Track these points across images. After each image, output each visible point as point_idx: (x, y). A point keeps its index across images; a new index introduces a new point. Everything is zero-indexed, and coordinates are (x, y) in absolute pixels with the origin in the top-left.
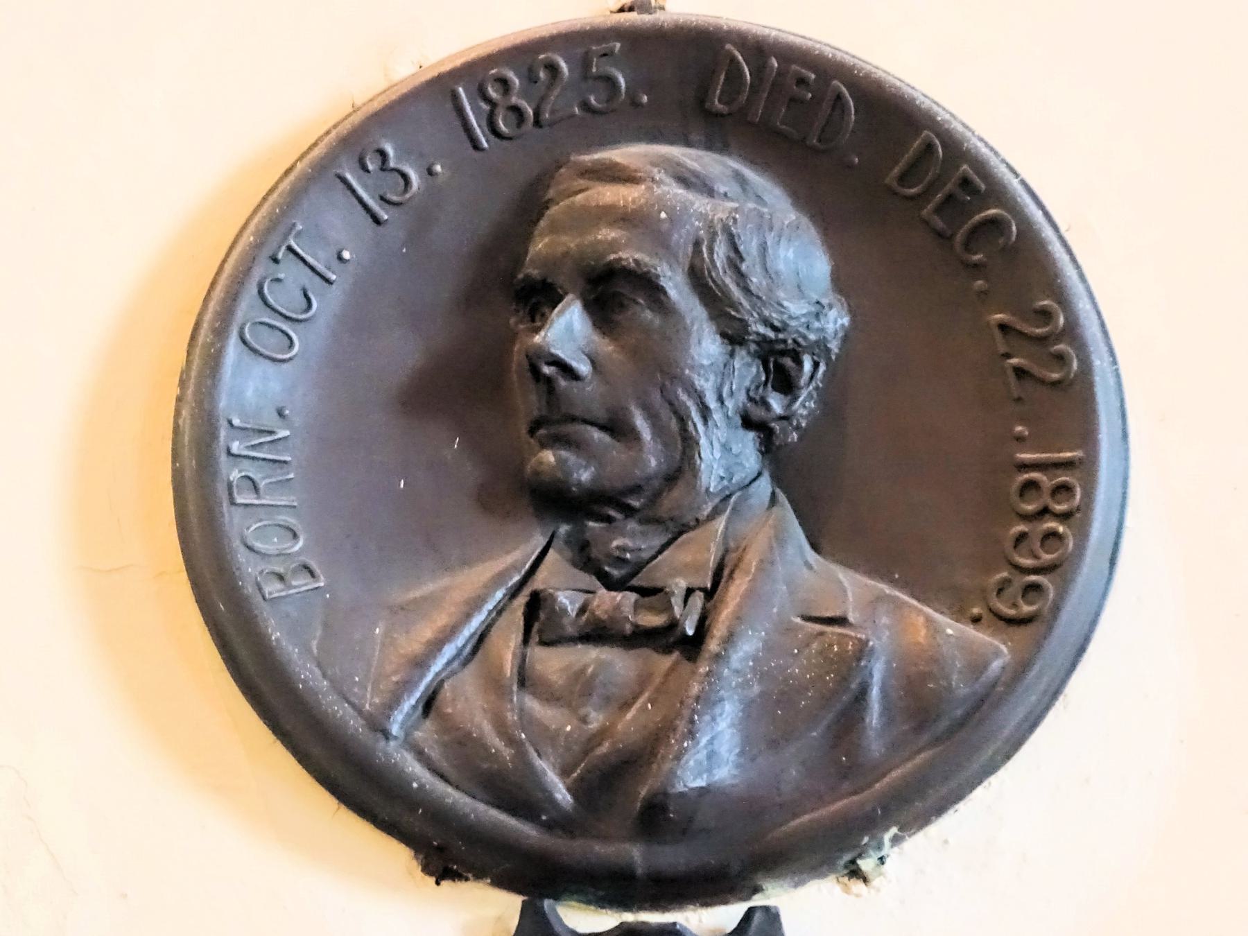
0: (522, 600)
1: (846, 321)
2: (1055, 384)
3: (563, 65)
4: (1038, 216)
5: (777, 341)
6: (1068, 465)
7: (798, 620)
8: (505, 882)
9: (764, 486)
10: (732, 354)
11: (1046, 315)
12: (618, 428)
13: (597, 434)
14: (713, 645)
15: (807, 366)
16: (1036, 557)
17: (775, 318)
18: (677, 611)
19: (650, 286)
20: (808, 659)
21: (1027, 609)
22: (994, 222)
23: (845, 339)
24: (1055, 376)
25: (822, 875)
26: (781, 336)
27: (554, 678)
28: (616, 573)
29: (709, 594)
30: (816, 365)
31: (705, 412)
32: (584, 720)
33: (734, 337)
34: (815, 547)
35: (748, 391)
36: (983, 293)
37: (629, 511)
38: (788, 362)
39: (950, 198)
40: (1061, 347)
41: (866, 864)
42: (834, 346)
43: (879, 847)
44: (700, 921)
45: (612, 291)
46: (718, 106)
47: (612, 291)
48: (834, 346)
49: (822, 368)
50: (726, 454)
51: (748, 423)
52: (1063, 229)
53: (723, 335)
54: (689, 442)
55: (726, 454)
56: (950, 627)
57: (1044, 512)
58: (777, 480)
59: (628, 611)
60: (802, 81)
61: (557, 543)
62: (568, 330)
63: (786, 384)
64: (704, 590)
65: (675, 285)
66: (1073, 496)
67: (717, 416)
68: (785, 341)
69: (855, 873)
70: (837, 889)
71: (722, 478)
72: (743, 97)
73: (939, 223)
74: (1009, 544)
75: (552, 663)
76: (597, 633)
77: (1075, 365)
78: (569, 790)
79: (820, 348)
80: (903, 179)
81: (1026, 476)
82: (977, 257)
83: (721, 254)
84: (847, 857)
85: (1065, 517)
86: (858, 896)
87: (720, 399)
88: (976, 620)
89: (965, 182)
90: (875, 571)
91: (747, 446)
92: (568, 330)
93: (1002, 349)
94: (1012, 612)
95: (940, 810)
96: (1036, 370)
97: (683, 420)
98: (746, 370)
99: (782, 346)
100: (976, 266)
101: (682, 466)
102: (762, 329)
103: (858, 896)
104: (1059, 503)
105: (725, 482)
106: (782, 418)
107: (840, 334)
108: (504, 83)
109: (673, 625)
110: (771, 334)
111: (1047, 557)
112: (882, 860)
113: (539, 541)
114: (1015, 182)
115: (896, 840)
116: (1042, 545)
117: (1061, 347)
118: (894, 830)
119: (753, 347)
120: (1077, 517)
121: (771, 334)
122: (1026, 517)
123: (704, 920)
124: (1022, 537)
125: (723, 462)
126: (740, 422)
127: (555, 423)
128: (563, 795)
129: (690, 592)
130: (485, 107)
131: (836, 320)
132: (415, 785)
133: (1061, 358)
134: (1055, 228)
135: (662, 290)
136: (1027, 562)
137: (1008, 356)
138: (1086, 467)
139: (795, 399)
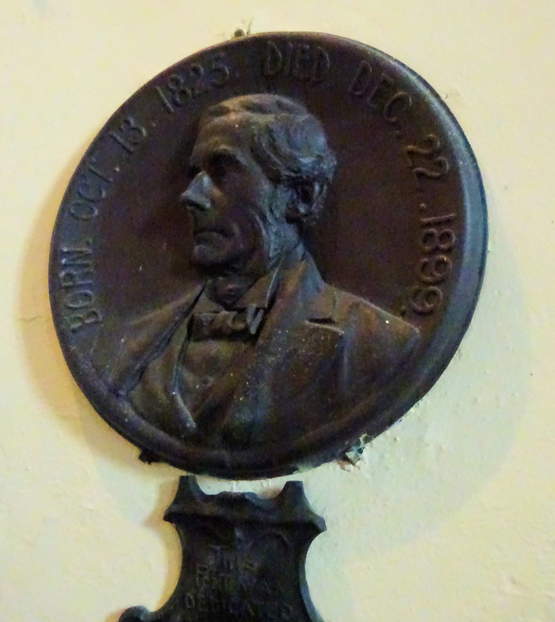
0: (187, 321)
1: (335, 162)
2: (436, 179)
3: (202, 70)
4: (427, 92)
5: (298, 178)
6: (449, 221)
7: (307, 322)
8: (174, 464)
9: (300, 250)
10: (276, 187)
11: (430, 142)
12: (225, 232)
13: (215, 234)
14: (261, 342)
15: (317, 188)
16: (432, 275)
17: (294, 167)
18: (249, 320)
19: (231, 160)
20: (310, 344)
21: (428, 306)
22: (399, 99)
23: (335, 173)
24: (437, 174)
25: (326, 460)
26: (299, 175)
27: (196, 358)
28: (229, 302)
29: (267, 311)
30: (322, 187)
31: (264, 218)
32: (205, 382)
33: (276, 180)
34: (324, 278)
35: (287, 204)
36: (399, 137)
37: (235, 270)
38: (307, 188)
39: (379, 90)
40: (441, 158)
41: (350, 455)
42: (330, 176)
43: (358, 443)
44: (268, 485)
45: (219, 165)
46: (270, 72)
47: (219, 165)
48: (330, 176)
49: (325, 187)
50: (277, 236)
51: (290, 220)
52: (443, 97)
53: (270, 179)
54: (257, 233)
55: (277, 236)
56: (388, 319)
57: (437, 250)
58: (307, 246)
59: (229, 322)
60: (303, 51)
61: (207, 290)
62: (202, 189)
63: (306, 197)
64: (264, 308)
65: (243, 158)
66: (451, 239)
67: (270, 219)
68: (301, 177)
69: (346, 459)
70: (338, 467)
71: (276, 250)
72: (280, 65)
73: (374, 106)
74: (418, 268)
75: (197, 349)
76: (218, 334)
77: (448, 166)
78: (195, 421)
79: (322, 178)
80: (355, 89)
81: (426, 230)
82: (394, 119)
83: (266, 141)
84: (340, 451)
85: (448, 251)
86: (349, 471)
87: (271, 211)
88: (403, 314)
89: (385, 82)
90: (356, 290)
91: (290, 233)
92: (202, 189)
93: (411, 164)
94: (420, 308)
95: (391, 422)
96: (429, 173)
97: (253, 222)
98: (284, 196)
99: (300, 180)
100: (394, 124)
101: (255, 246)
102: (287, 173)
103: (349, 471)
104: (443, 244)
105: (279, 251)
106: (306, 216)
107: (333, 170)
108: (177, 82)
109: (246, 330)
110: (293, 175)
111: (438, 275)
112: (360, 451)
113: (199, 288)
114: (413, 78)
115: (367, 440)
116: (436, 269)
117: (441, 158)
118: (364, 436)
119: (286, 183)
120: (455, 251)
121: (293, 175)
122: (426, 254)
123: (270, 484)
124: (425, 265)
125: (278, 241)
126: (284, 219)
127: (199, 232)
128: (191, 423)
129: (257, 310)
130: (170, 94)
131: (329, 164)
132: (126, 420)
133: (441, 164)
134: (437, 96)
135: (238, 162)
136: (429, 279)
137: (413, 167)
138: (458, 222)
139: (311, 206)
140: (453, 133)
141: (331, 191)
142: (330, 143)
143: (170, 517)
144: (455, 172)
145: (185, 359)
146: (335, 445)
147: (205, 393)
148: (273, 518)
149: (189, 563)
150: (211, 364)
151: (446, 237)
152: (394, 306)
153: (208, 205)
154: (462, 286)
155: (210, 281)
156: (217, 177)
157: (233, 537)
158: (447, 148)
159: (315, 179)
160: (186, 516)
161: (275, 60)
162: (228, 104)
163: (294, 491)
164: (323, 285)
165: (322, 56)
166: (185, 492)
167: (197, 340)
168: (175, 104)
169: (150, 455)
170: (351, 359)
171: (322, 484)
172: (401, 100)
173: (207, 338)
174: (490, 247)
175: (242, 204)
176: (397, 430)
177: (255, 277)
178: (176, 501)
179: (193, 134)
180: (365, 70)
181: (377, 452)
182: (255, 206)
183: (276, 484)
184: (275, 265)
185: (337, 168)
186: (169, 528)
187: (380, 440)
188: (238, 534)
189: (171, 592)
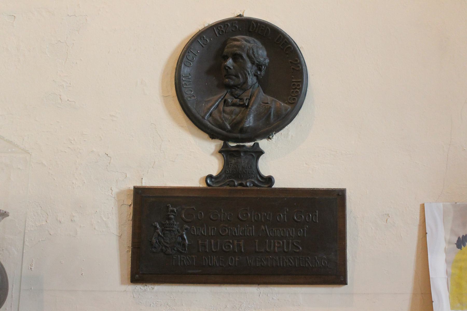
6: (299, 82)
9: (257, 84)
11: (297, 61)
12: (237, 76)
28: (236, 96)
31: (249, 74)
33: (253, 63)
34: (264, 93)
37: (238, 88)
41: (271, 137)
42: (267, 65)
45: (236, 57)
46: (251, 30)
48: (267, 65)
50: (251, 80)
51: (255, 75)
54: (247, 78)
55: (251, 80)
57: (296, 88)
58: (259, 84)
60: (263, 27)
63: (260, 70)
65: (245, 56)
75: (228, 109)
79: (265, 65)
82: (287, 52)
85: (299, 89)
88: (286, 103)
89: (286, 42)
90: (273, 97)
91: (255, 79)
92: (230, 62)
97: (246, 75)
98: (255, 68)
101: (246, 82)
108: (221, 27)
109: (244, 104)
113: (226, 92)
115: (275, 134)
122: (294, 89)
124: (293, 92)
127: (228, 75)
128: (229, 127)
129: (247, 99)
131: (267, 61)
133: (299, 67)
136: (293, 95)
140: (302, 59)
141: (267, 68)
142: (268, 56)
143: (220, 152)
144: (302, 69)
145: (224, 111)
146: (267, 135)
147: (233, 120)
148: (251, 150)
149: (226, 164)
150: (231, 113)
151: (299, 85)
152: (284, 101)
153: (232, 68)
154: (301, 99)
155: (229, 90)
156: (235, 60)
157: (241, 155)
158: (300, 63)
159: (264, 65)
160: (225, 152)
161: (253, 27)
162: (238, 37)
163: (258, 144)
164: (264, 94)
165: (268, 29)
166: (225, 145)
167: (227, 106)
168: (219, 33)
169: (213, 135)
170: (273, 113)
171: (263, 144)
172: (290, 48)
173: (230, 106)
174: (308, 89)
175: (243, 68)
176: (282, 131)
177: (245, 90)
178: (223, 147)
179: (224, 44)
180: (281, 37)
181: (276, 137)
182: (247, 70)
183: (251, 144)
184: (250, 88)
185: (269, 63)
186: (219, 156)
187: (278, 134)
188: (242, 154)
189: (220, 171)
